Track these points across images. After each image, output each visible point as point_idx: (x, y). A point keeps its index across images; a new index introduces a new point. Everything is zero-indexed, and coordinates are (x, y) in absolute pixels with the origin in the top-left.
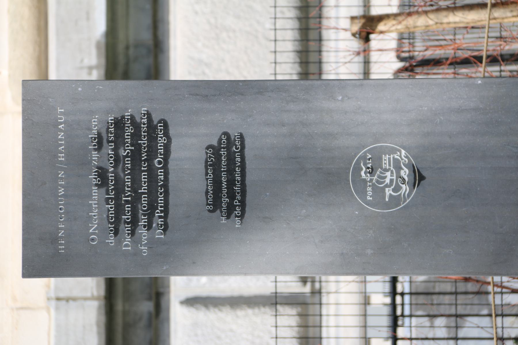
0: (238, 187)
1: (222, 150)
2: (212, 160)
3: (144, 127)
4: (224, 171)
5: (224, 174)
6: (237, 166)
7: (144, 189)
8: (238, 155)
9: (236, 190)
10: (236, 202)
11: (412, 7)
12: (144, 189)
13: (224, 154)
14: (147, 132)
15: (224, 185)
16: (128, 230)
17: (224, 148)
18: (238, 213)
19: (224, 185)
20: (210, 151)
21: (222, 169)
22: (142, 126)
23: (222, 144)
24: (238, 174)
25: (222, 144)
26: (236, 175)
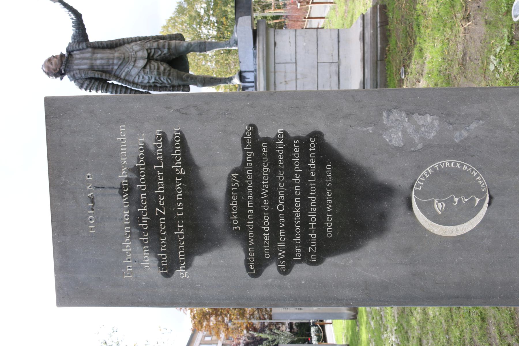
7: (161, 190)
8: (281, 216)
12: (161, 190)
13: (281, 152)
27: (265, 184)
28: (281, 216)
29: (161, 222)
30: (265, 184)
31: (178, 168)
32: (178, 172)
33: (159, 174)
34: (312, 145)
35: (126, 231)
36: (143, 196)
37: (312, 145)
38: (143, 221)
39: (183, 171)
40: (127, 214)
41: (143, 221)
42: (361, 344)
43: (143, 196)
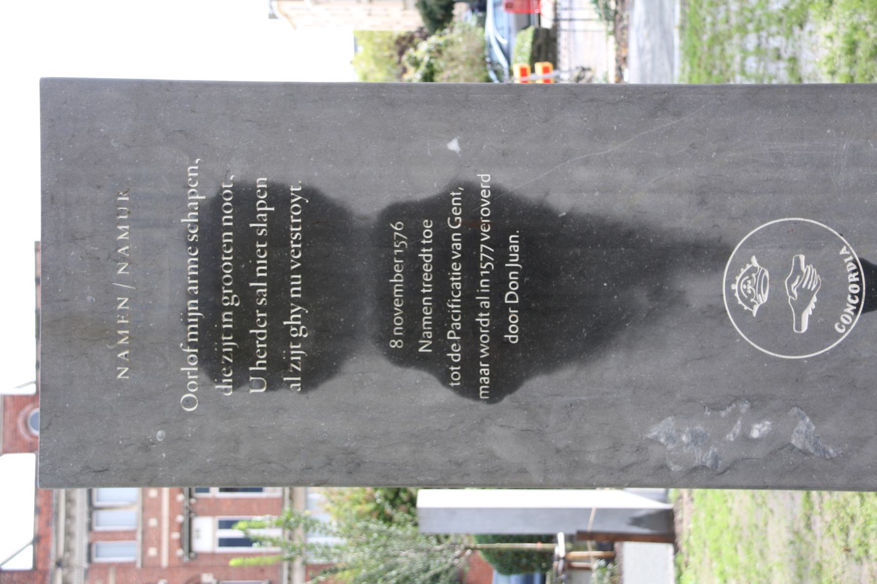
0: (455, 303)
1: (424, 250)
2: (403, 245)
3: (295, 232)
4: (427, 294)
5: (426, 301)
6: (455, 260)
7: (261, 365)
8: (456, 237)
9: (451, 309)
10: (451, 335)
11: (844, 537)
12: (261, 365)
13: (427, 258)
14: (303, 241)
15: (427, 269)
16: (193, 329)
17: (427, 246)
18: (456, 358)
19: (427, 269)
20: (399, 226)
21: (424, 291)
22: (292, 229)
23: (423, 238)
24: (456, 276)
25: (423, 238)
26: (453, 279)
27: (455, 281)
28: (456, 237)
29: (225, 241)
30: (455, 281)
31: (294, 326)
32: (294, 332)
33: (259, 315)
34: (428, 234)
35: (190, 273)
36: (227, 237)
37: (428, 234)
38: (196, 320)
39: (304, 332)
40: (226, 201)
41: (196, 320)
42: (417, 5)
43: (227, 237)
